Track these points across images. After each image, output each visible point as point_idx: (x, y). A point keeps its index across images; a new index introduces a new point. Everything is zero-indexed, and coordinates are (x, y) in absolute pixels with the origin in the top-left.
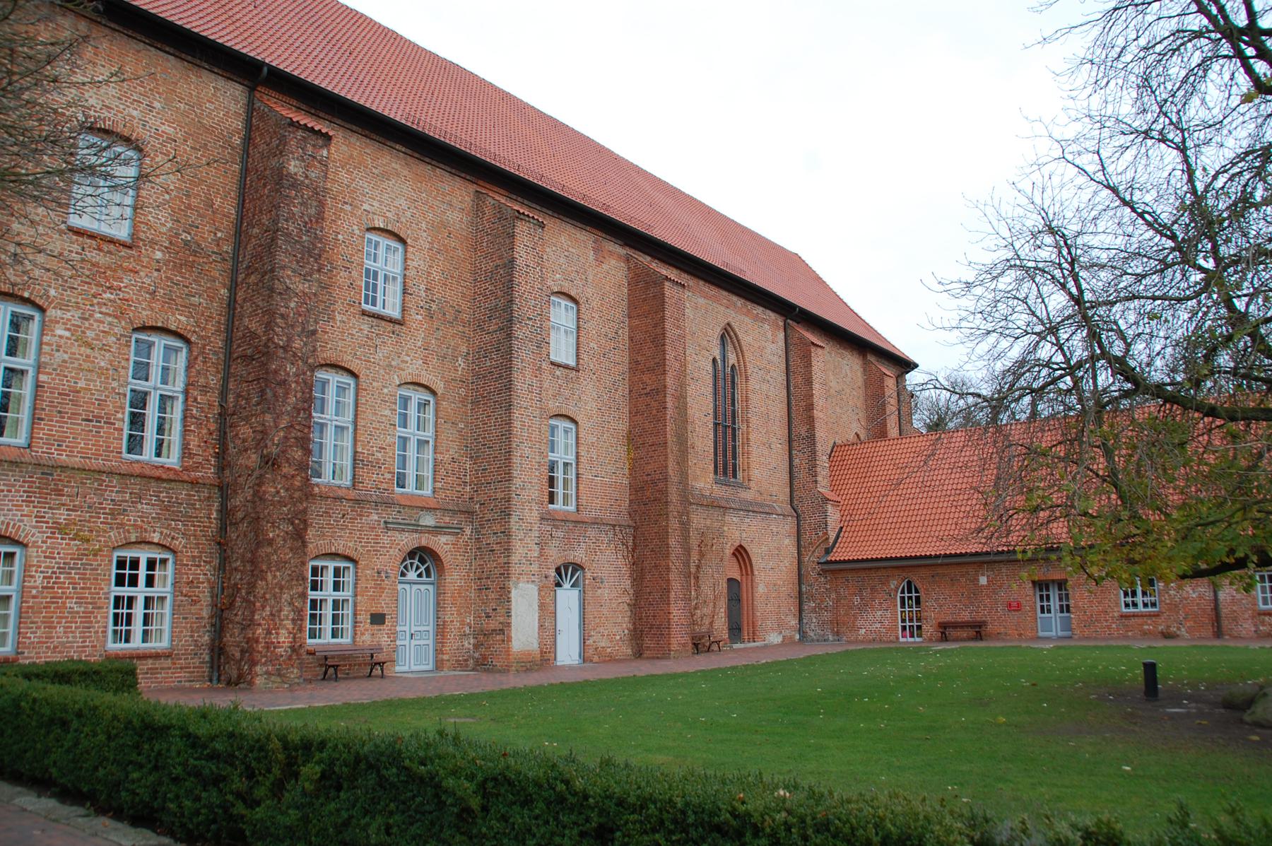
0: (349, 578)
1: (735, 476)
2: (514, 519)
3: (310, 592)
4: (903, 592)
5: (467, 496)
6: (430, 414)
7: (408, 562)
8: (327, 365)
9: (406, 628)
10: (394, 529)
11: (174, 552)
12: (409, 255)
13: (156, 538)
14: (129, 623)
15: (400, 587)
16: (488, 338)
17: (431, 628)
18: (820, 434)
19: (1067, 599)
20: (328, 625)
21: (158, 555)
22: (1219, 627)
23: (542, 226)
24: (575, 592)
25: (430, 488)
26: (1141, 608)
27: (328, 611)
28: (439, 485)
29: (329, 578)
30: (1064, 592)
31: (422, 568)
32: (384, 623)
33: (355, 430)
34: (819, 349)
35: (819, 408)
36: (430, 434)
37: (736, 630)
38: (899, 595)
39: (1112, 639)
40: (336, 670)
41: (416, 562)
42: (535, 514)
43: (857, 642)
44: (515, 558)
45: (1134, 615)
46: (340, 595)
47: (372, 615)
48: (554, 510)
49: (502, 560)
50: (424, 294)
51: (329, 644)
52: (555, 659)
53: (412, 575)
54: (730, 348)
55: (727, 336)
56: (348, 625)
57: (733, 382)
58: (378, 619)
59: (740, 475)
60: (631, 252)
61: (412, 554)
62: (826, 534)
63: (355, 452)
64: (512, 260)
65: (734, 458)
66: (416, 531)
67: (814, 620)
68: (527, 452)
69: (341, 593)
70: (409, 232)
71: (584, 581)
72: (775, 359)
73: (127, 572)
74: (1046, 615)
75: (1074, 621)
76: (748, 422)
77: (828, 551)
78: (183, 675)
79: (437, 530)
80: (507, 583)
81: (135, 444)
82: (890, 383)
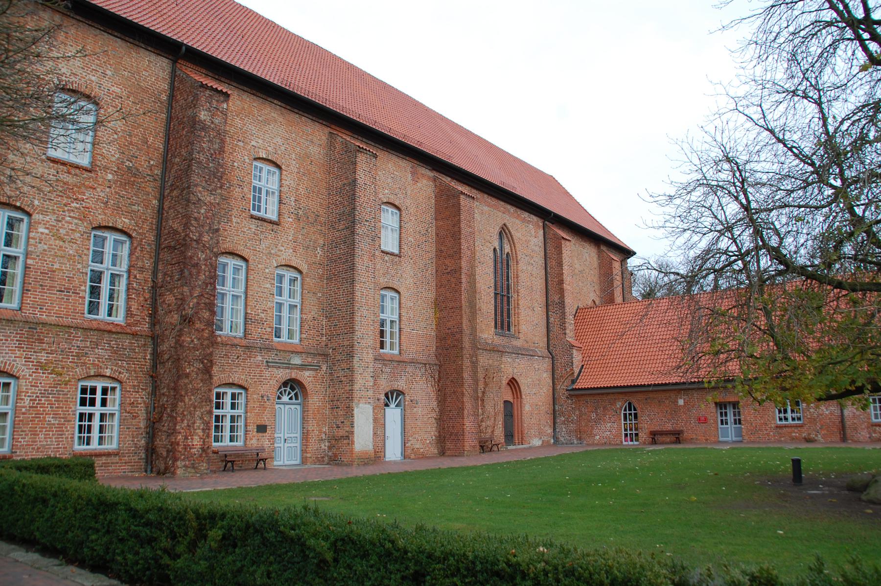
0: (242, 401)
1: (509, 330)
2: (356, 359)
3: (215, 410)
4: (625, 410)
5: (323, 344)
6: (298, 287)
7: (283, 389)
8: (226, 253)
9: (281, 435)
10: (273, 367)
11: (120, 382)
12: (283, 177)
13: (108, 372)
14: (89, 431)
15: (277, 406)
16: (338, 234)
17: (298, 435)
18: (568, 300)
19: (739, 415)
20: (227, 433)
21: (109, 384)
22: (844, 434)
23: (375, 156)
24: (398, 410)
25: (298, 338)
27: (227, 424)
28: (304, 336)
29: (228, 400)
30: (737, 410)
31: (293, 394)
32: (266, 432)
33: (246, 298)
34: (567, 242)
35: (567, 283)
36: (298, 301)
37: (509, 437)
38: (623, 412)
39: (770, 442)
40: (232, 464)
41: (288, 389)
42: (371, 356)
43: (593, 444)
44: (356, 387)
45: (786, 426)
46: (235, 412)
47: (257, 426)
48: (383, 353)
49: (348, 388)
50: (294, 204)
51: (228, 446)
52: (385, 457)
53: (285, 398)
54: (505, 241)
55: (504, 232)
56: (241, 433)
57: (508, 265)
58: (262, 429)
59: (512, 329)
60: (437, 174)
61: (285, 384)
62: (572, 370)
63: (246, 313)
64: (355, 180)
65: (509, 317)
66: (288, 368)
67: (564, 430)
68: (365, 313)
69: (236, 411)
70: (283, 161)
71: (404, 402)
72: (537, 249)
73: (88, 396)
74: (725, 426)
75: (744, 430)
76: (518, 292)
77: (573, 382)
79: (302, 367)
80: (351, 404)
82: (617, 265)
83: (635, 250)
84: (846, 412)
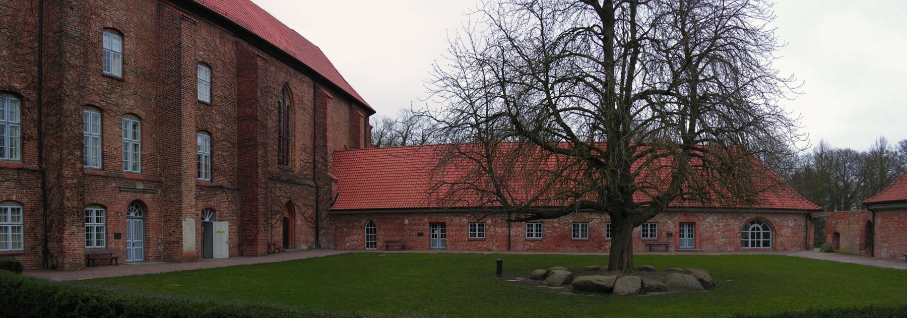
0: (103, 216)
1: (287, 165)
2: (183, 185)
4: (368, 226)
5: (158, 173)
6: (138, 131)
7: (131, 207)
9: (131, 241)
10: (124, 191)
11: (23, 205)
12: (126, 42)
13: (14, 198)
16: (167, 87)
18: (330, 145)
19: (445, 232)
20: (94, 240)
22: (509, 246)
23: (195, 23)
25: (140, 169)
26: (534, 237)
28: (144, 168)
29: (94, 216)
31: (137, 211)
32: (121, 238)
33: (103, 139)
34: (331, 99)
35: (329, 131)
36: (139, 141)
37: (286, 243)
38: (366, 227)
39: (464, 250)
40: (93, 261)
41: (134, 207)
42: (194, 182)
43: (345, 249)
44: (184, 206)
45: (474, 240)
47: (115, 234)
48: (200, 180)
49: (177, 206)
51: (95, 248)
53: (133, 214)
54: (286, 96)
55: (286, 88)
57: (288, 115)
58: (118, 236)
59: (290, 164)
60: (238, 39)
61: (132, 204)
62: (331, 196)
63: (103, 152)
64: (181, 43)
65: (288, 155)
66: (134, 192)
67: (324, 239)
68: (189, 149)
69: (100, 224)
71: (215, 217)
72: (308, 103)
74: (682, 238)
75: (447, 242)
76: (295, 136)
77: (332, 205)
78: (31, 263)
79: (144, 191)
80: (180, 218)
81: (11, 157)
82: (362, 120)
83: (373, 106)
84: (512, 233)
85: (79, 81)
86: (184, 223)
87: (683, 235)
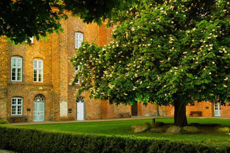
0: (22, 101)
3: (12, 104)
8: (15, 56)
9: (37, 112)
14: (15, 111)
15: (35, 103)
17: (43, 112)
20: (17, 111)
21: (20, 98)
24: (83, 104)
27: (17, 108)
29: (17, 101)
31: (41, 99)
46: (19, 105)
52: (77, 119)
56: (22, 111)
58: (29, 110)
68: (64, 72)
74: (216, 110)
79: (43, 90)
85: (6, 48)
86: (60, 104)
87: (217, 108)
